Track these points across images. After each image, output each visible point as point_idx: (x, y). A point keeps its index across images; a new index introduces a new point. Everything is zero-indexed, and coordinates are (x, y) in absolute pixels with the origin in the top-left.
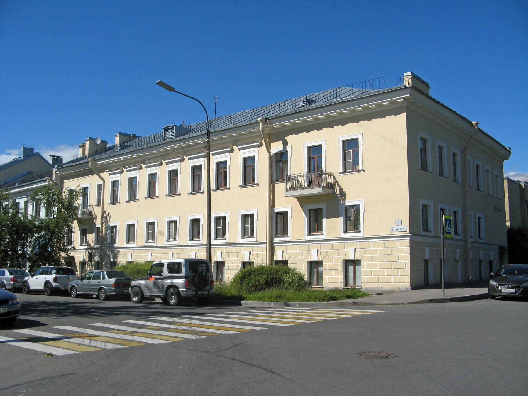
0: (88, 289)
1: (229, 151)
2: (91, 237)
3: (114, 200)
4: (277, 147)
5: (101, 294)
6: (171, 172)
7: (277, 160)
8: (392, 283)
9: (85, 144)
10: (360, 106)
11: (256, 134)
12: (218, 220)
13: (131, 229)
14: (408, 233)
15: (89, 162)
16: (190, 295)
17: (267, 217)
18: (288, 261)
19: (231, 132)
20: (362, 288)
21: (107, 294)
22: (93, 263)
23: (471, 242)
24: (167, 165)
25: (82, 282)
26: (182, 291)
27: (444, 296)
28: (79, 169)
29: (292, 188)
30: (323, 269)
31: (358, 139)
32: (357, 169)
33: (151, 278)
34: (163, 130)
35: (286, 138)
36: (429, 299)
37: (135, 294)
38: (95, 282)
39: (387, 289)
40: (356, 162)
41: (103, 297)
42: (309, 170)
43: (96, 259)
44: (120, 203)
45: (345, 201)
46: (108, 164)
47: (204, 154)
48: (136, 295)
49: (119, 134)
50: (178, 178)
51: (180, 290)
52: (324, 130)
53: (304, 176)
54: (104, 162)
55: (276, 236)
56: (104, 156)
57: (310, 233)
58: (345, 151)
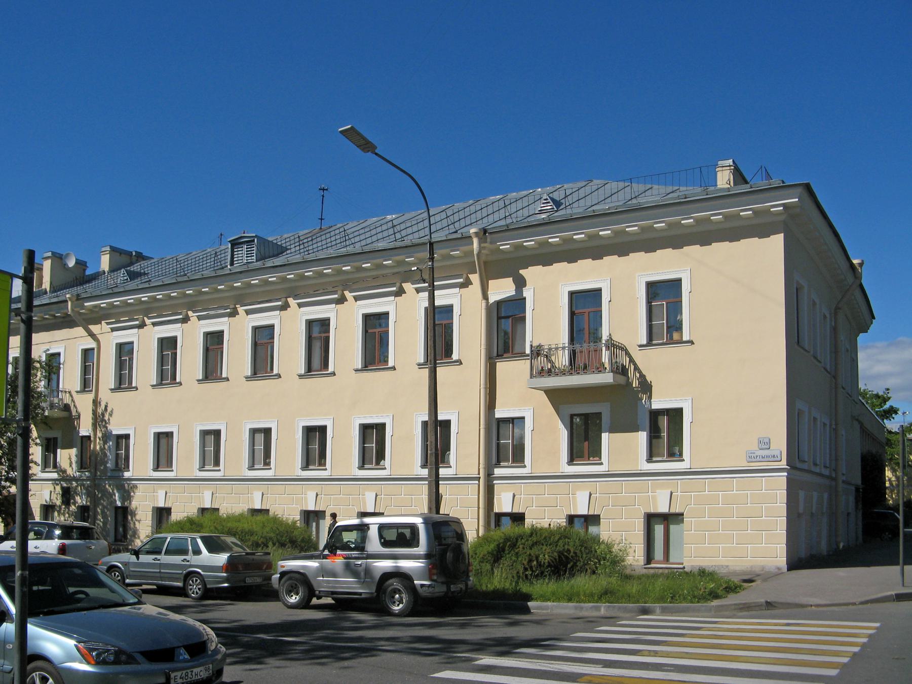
0: (155, 575)
1: (395, 292)
2: (67, 457)
3: (123, 382)
4: (501, 289)
5: (191, 585)
6: (208, 336)
7: (499, 315)
8: (749, 558)
9: (43, 265)
10: (692, 215)
11: (273, 287)
12: (365, 430)
13: (163, 441)
14: (783, 464)
15: (66, 301)
16: (439, 593)
17: (481, 427)
18: (524, 514)
19: (447, 248)
20: (684, 568)
21: (208, 586)
22: (73, 508)
23: (843, 482)
24: (247, 315)
25: (138, 558)
26: (422, 586)
27: (903, 585)
28: (38, 315)
29: (542, 373)
30: (601, 530)
31: (601, 290)
32: (674, 339)
33: (335, 555)
34: (230, 245)
35: (521, 272)
36: (894, 594)
37: (290, 588)
38: (177, 559)
39: (738, 568)
40: (675, 326)
41: (197, 593)
42: (572, 339)
43: (81, 500)
44: (137, 389)
45: (652, 400)
46: (110, 309)
47: (336, 296)
48: (291, 592)
49: (109, 249)
50: (223, 348)
51: (415, 582)
52: (556, 266)
53: (564, 348)
54: (103, 303)
55: (498, 464)
56: (101, 292)
57: (571, 461)
58: (652, 303)
